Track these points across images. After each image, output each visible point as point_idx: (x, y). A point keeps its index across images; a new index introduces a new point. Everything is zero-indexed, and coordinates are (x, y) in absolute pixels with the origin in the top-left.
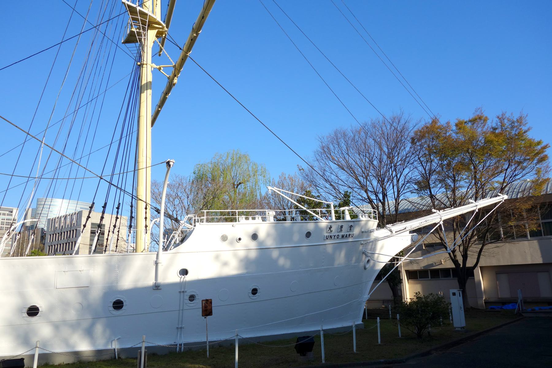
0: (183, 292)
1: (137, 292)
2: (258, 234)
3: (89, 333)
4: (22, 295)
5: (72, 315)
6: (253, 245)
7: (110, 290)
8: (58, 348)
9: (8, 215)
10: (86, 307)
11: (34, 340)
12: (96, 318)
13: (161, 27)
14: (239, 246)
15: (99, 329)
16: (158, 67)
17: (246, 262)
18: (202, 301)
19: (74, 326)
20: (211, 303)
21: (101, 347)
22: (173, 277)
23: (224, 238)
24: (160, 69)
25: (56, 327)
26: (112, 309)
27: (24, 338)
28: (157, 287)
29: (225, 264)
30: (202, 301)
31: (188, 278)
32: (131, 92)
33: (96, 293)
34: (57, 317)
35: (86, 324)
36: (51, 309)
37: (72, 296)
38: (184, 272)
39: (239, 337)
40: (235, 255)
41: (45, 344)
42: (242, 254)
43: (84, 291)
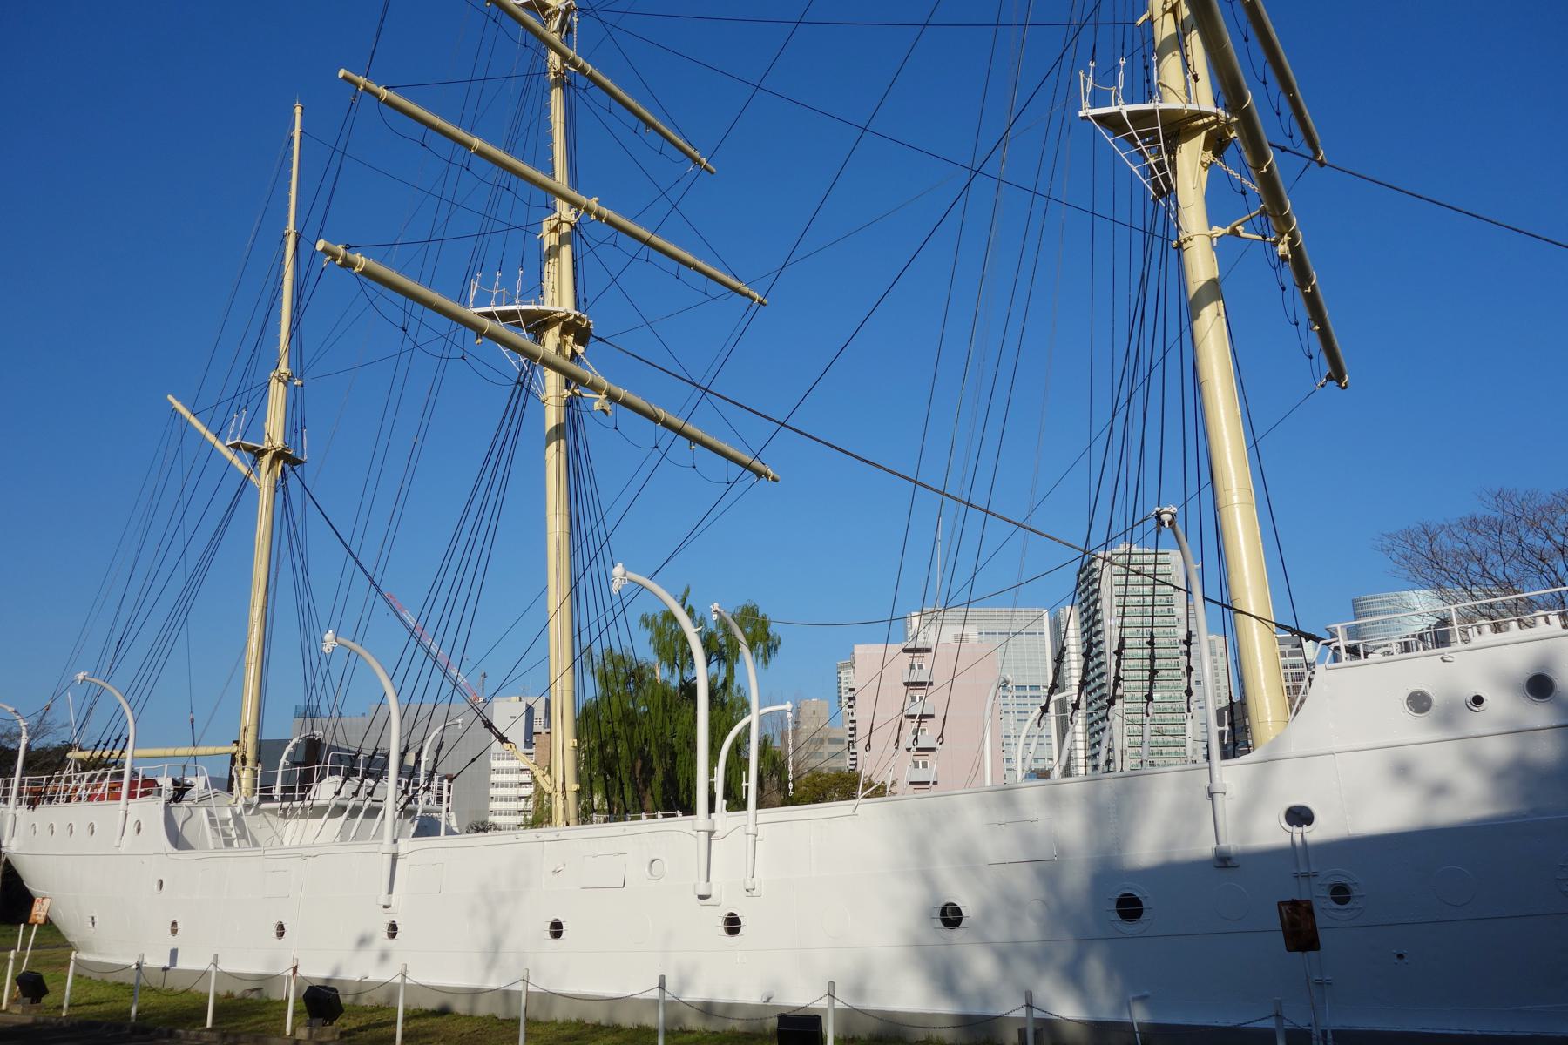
0: (1306, 875)
1: (1172, 873)
2: (1527, 677)
3: (1073, 976)
4: (928, 879)
5: (1030, 931)
6: (1540, 715)
7: (1106, 870)
8: (1010, 1007)
9: (1292, 654)
10: (1059, 914)
11: (966, 985)
12: (1084, 941)
13: (1212, 118)
14: (1477, 723)
15: (1095, 969)
16: (1228, 229)
17: (1518, 775)
18: (1280, 904)
19: (1041, 959)
20: (1310, 911)
21: (1106, 1015)
22: (1271, 832)
23: (1419, 702)
24: (1234, 232)
25: (1004, 957)
26: (1116, 917)
27: (946, 978)
28: (1223, 861)
29: (1439, 790)
30: (1280, 904)
31: (1313, 834)
32: (484, 504)
33: (1076, 879)
34: (1000, 932)
35: (1064, 952)
36: (987, 914)
37: (1024, 883)
38: (1299, 816)
39: (1287, 1025)
40: (1473, 760)
41: (985, 995)
42: (1498, 749)
43: (1048, 870)
